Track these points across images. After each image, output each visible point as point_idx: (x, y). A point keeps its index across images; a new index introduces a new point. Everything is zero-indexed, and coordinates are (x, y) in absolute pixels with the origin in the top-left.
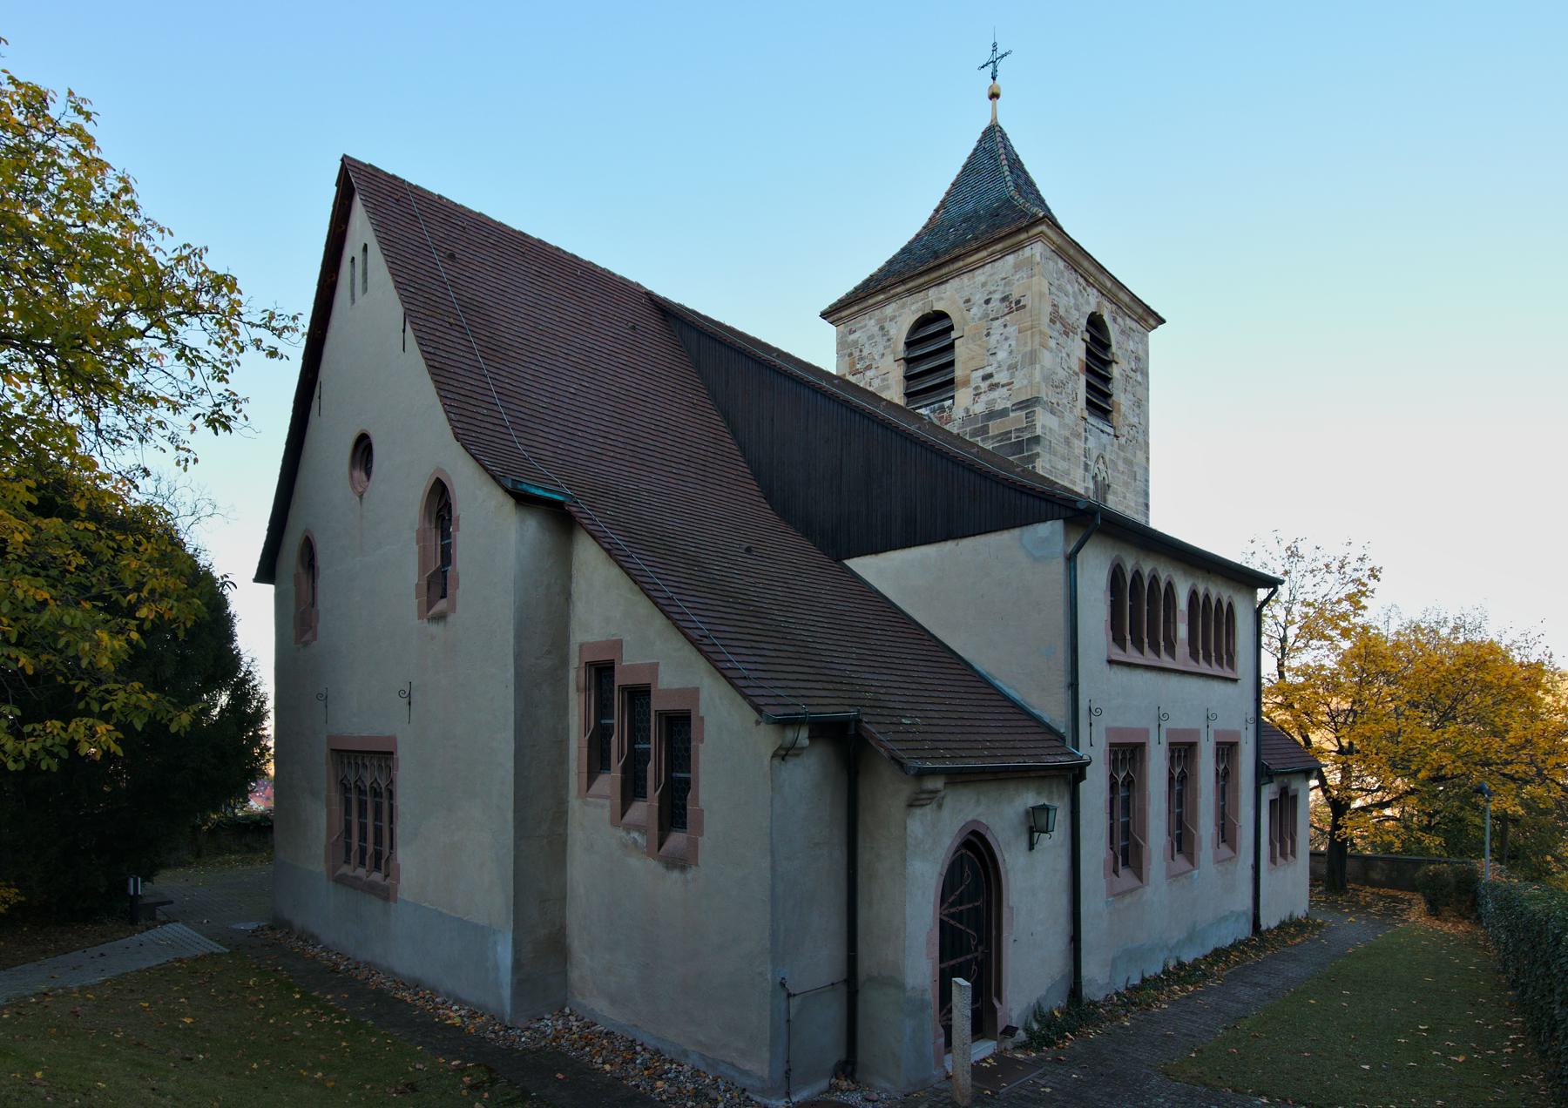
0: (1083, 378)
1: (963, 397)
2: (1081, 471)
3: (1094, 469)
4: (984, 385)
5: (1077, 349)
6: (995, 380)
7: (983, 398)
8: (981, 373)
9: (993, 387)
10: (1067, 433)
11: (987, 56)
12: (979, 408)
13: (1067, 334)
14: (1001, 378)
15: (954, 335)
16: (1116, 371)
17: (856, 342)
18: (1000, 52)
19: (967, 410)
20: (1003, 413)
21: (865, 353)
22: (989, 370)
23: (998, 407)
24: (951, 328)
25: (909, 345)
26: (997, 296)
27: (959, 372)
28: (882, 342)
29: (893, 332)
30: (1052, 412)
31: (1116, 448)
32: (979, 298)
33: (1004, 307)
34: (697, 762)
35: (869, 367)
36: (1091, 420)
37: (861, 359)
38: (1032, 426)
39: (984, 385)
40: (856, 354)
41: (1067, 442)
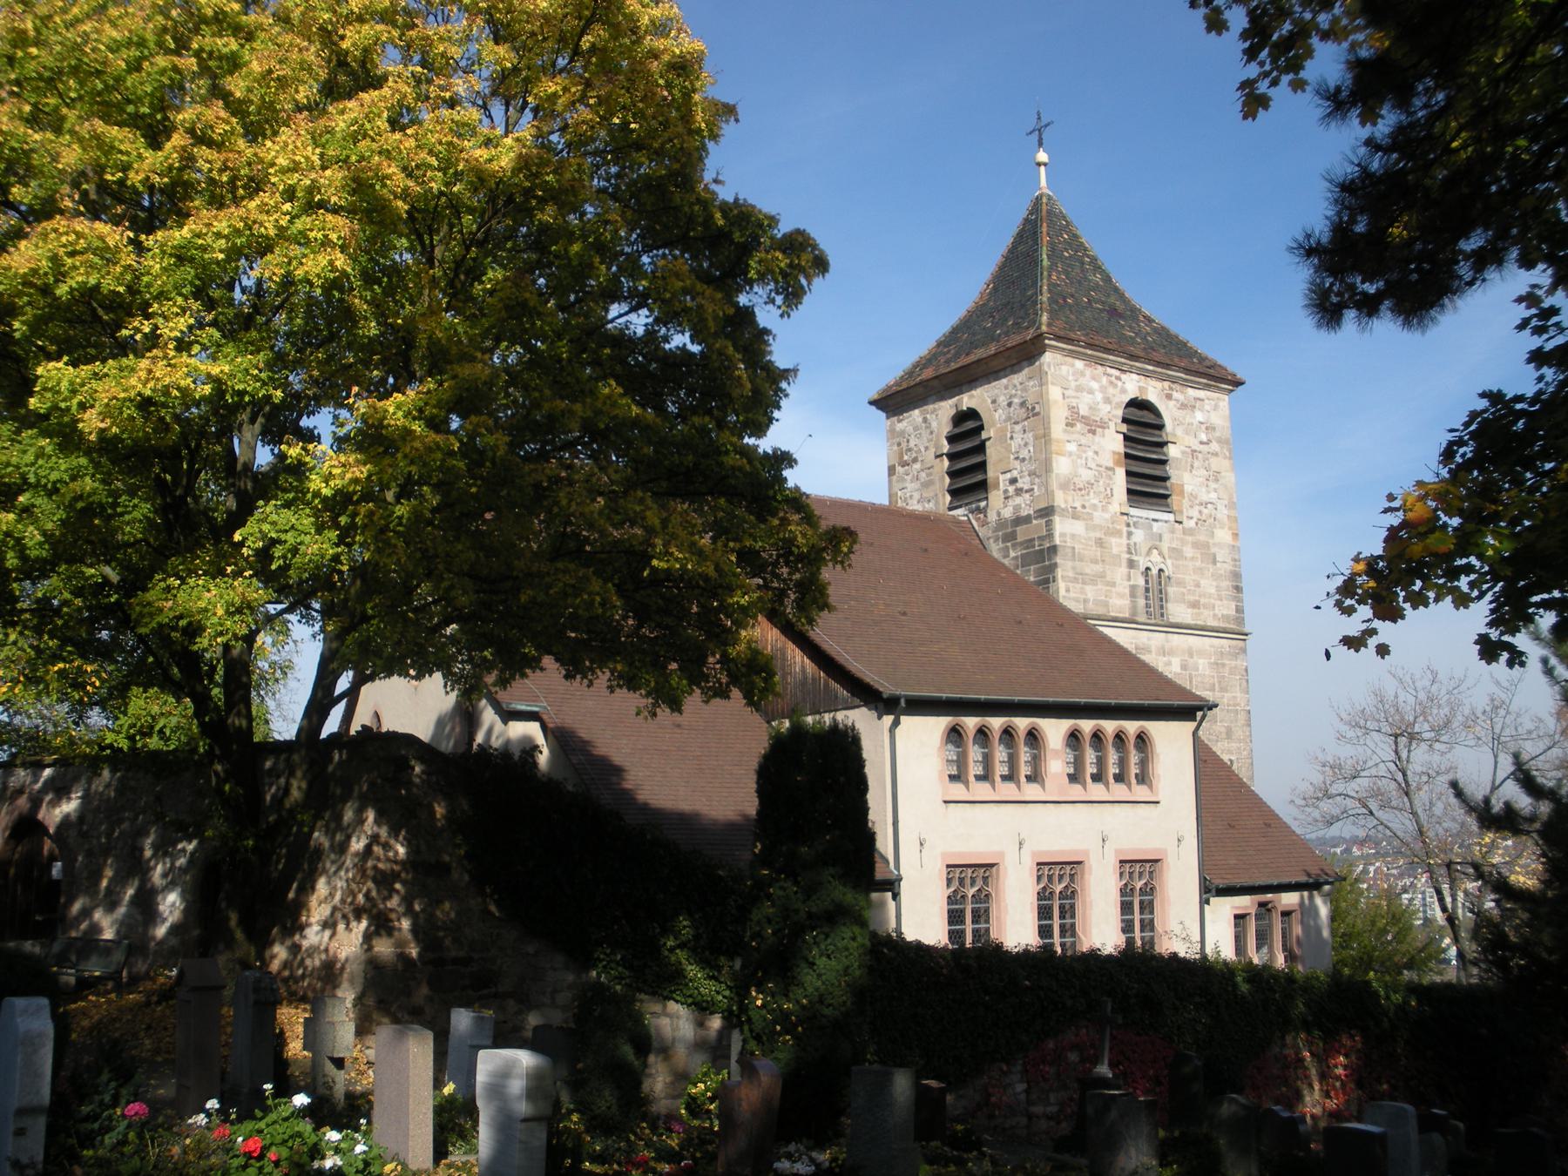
0: (1121, 473)
1: (995, 498)
2: (1124, 570)
3: (1142, 562)
4: (1011, 489)
5: (1113, 442)
6: (1019, 485)
7: (1011, 502)
8: (1008, 476)
9: (1019, 492)
10: (1098, 535)
11: (1032, 123)
12: (1008, 513)
13: (1094, 432)
14: (1024, 483)
15: (984, 435)
16: (1172, 451)
17: (902, 433)
18: (1044, 121)
19: (999, 514)
20: (1027, 520)
21: (912, 444)
22: (1015, 473)
23: (1024, 513)
24: (981, 428)
25: (952, 439)
26: (1016, 400)
27: (991, 472)
28: (925, 434)
29: (934, 424)
30: (1075, 517)
31: (1179, 534)
32: (1003, 400)
33: (1022, 413)
34: (1062, 852)
35: (915, 460)
36: (1133, 511)
37: (910, 450)
38: (1050, 536)
39: (1011, 489)
40: (904, 445)
41: (1100, 543)
